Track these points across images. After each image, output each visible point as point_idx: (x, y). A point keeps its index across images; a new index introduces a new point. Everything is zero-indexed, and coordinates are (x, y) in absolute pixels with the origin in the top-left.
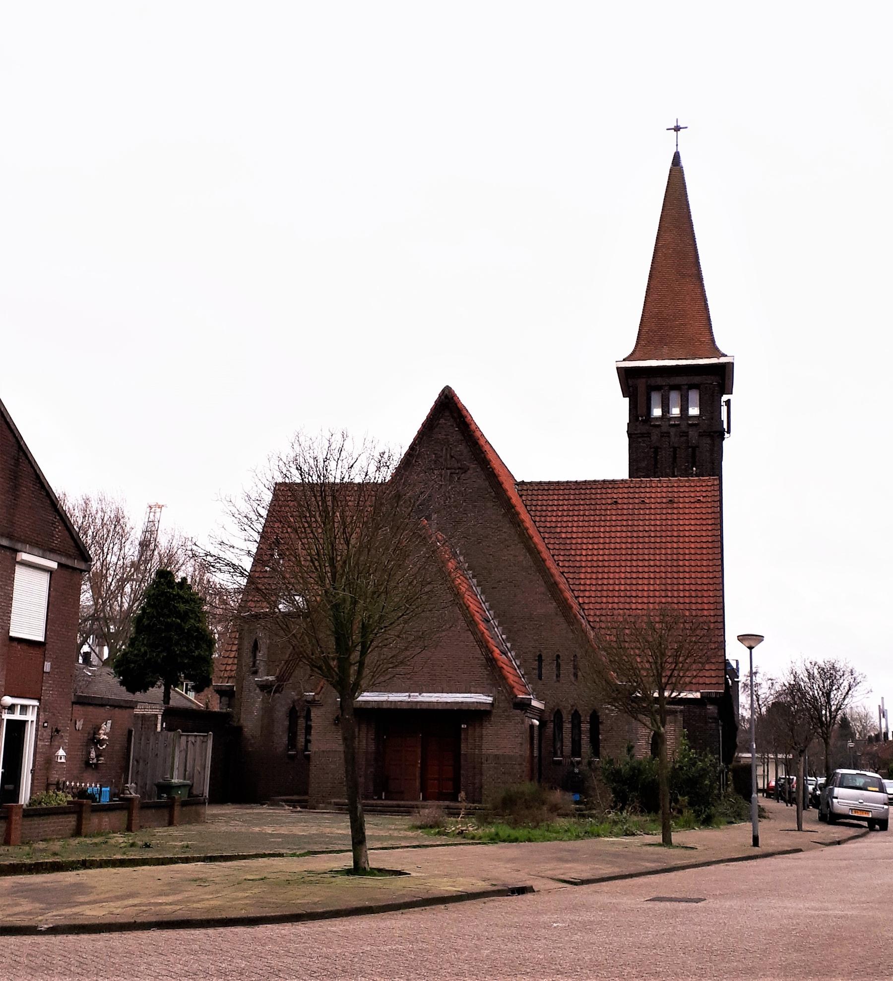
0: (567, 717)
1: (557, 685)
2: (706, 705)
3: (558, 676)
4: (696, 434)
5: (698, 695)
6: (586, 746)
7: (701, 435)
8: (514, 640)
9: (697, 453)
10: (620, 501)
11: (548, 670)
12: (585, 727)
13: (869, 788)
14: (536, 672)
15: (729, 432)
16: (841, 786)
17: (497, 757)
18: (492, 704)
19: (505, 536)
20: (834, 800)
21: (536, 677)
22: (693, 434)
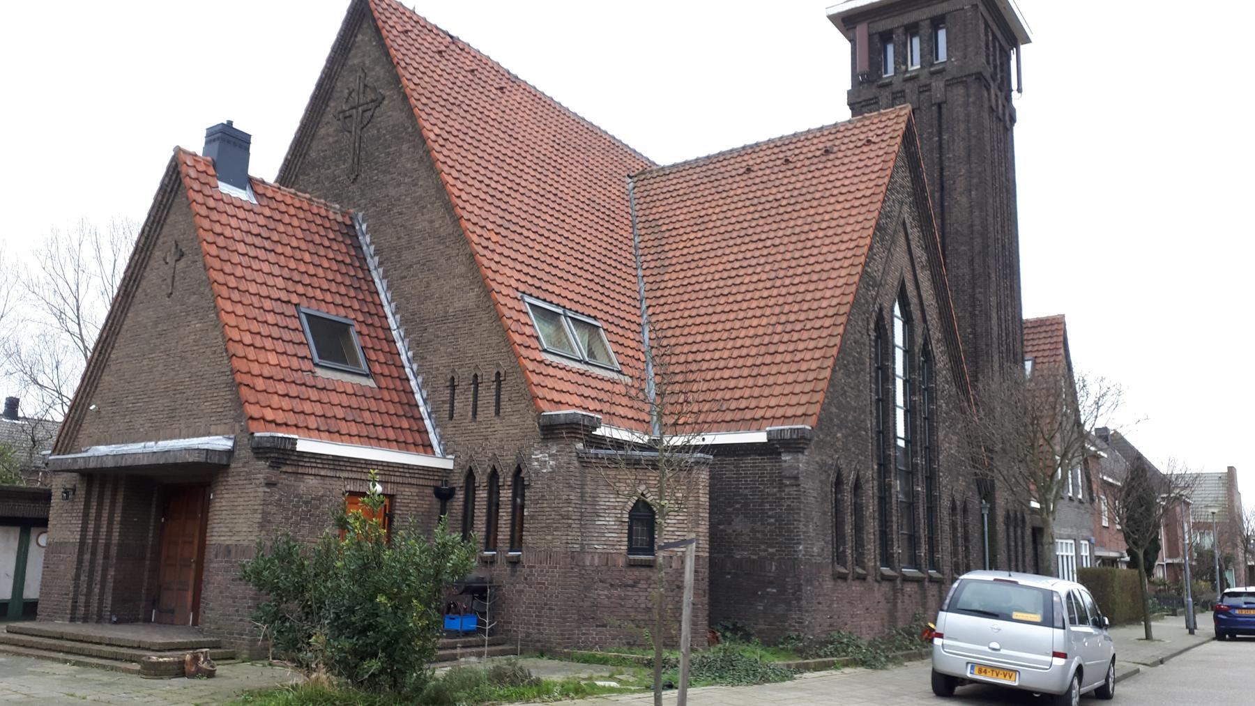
0: (481, 479)
1: (473, 426)
2: (780, 454)
3: (475, 413)
4: (942, 84)
5: (760, 437)
6: (504, 533)
7: (949, 85)
8: (423, 358)
9: (944, 110)
10: (755, 168)
11: (463, 404)
12: (506, 494)
13: (1016, 615)
14: (447, 406)
15: (1019, 90)
16: (954, 608)
17: (228, 550)
18: (230, 453)
19: (420, 192)
20: (937, 641)
21: (446, 415)
22: (938, 85)
